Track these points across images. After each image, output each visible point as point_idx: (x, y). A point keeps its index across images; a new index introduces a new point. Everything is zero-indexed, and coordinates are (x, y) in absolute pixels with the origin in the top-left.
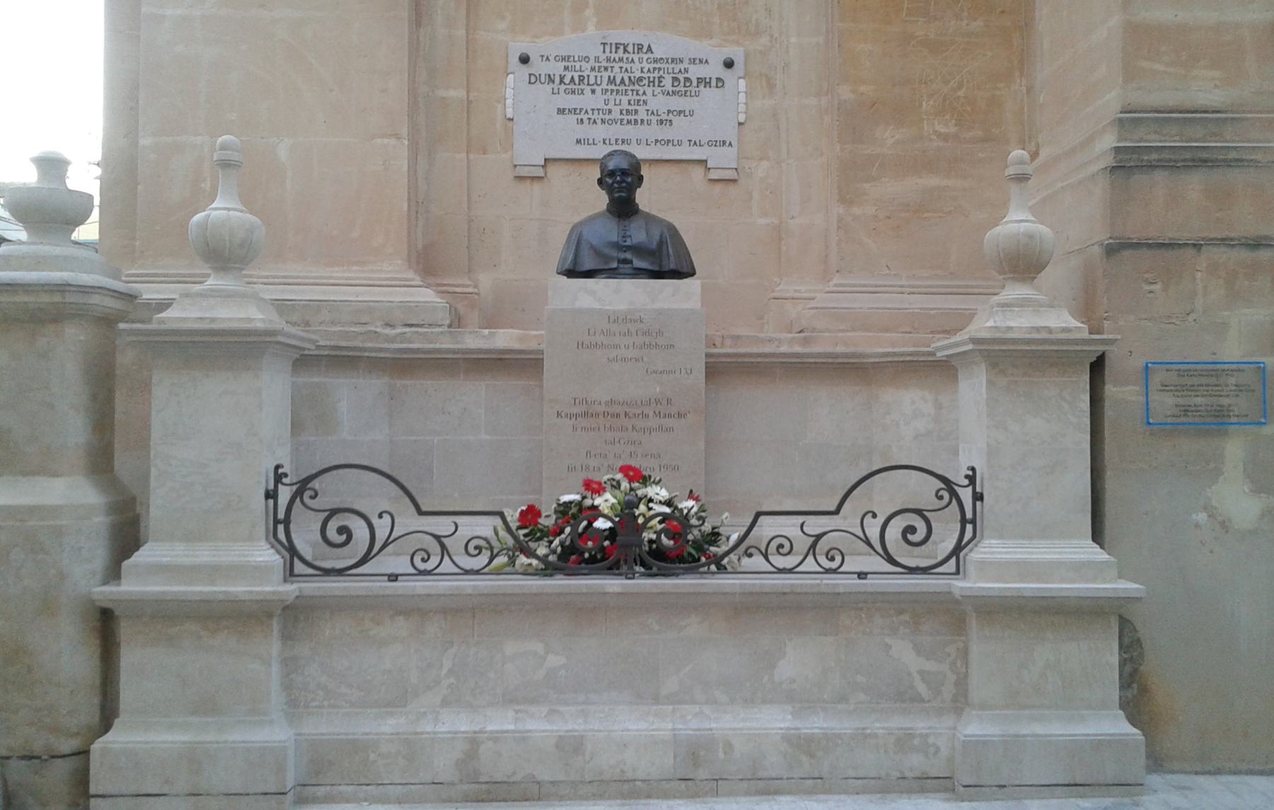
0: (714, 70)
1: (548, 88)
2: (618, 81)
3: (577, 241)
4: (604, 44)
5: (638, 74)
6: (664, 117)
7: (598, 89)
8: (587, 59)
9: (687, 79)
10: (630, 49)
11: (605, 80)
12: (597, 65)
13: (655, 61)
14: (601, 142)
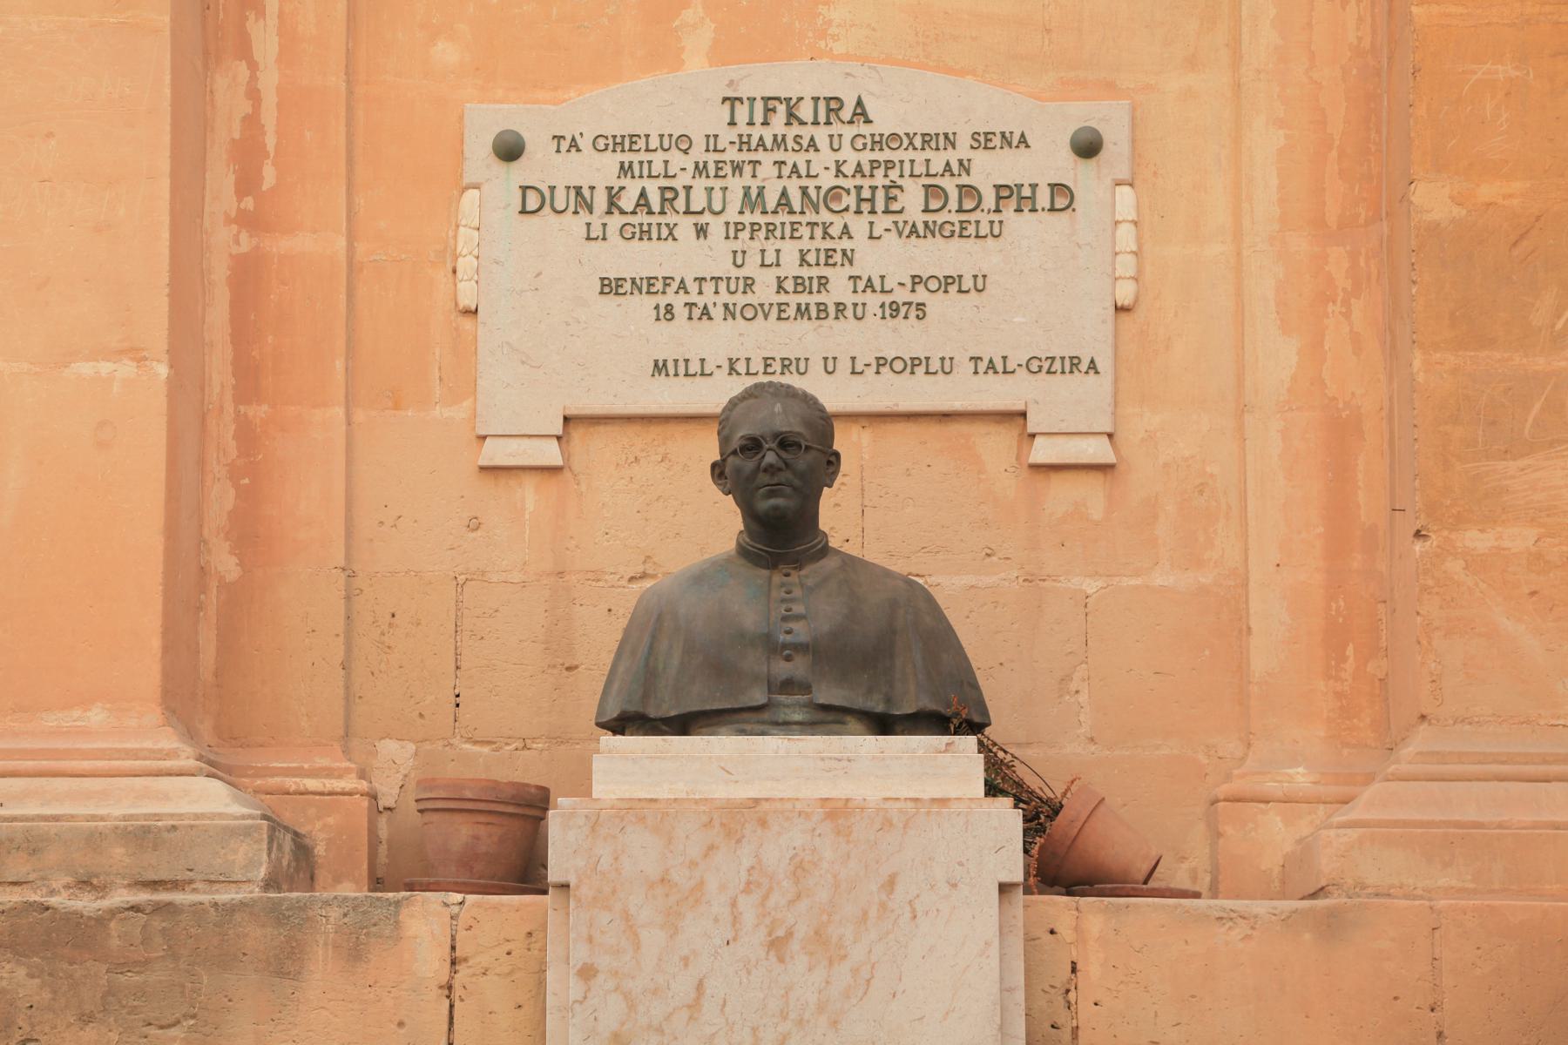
0: (1049, 160)
1: (575, 224)
2: (771, 200)
3: (651, 631)
4: (732, 101)
5: (827, 180)
6: (901, 296)
7: (716, 226)
8: (683, 143)
9: (967, 190)
10: (805, 112)
11: (736, 198)
12: (712, 157)
13: (878, 143)
14: (720, 363)
